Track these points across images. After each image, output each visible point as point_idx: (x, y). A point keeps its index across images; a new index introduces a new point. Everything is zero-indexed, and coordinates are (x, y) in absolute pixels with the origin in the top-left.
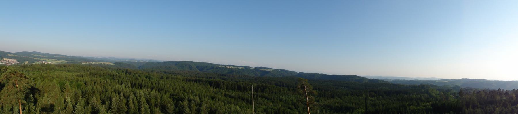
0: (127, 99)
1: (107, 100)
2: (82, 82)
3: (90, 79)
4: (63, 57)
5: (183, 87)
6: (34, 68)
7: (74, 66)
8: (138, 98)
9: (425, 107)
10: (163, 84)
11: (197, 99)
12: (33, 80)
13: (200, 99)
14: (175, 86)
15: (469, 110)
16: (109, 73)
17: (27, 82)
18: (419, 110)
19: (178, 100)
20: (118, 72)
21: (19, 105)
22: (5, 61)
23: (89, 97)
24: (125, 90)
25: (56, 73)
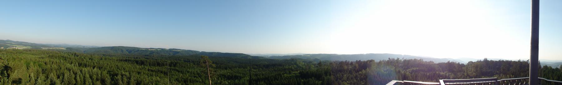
1: (61, 75)
3: (49, 60)
5: (117, 66)
6: (7, 52)
7: (36, 51)
8: (84, 74)
9: (295, 75)
10: (102, 64)
11: (127, 74)
12: (7, 60)
13: (129, 74)
15: (327, 77)
17: (2, 62)
18: (291, 76)
19: (113, 75)
20: (69, 55)
25: (23, 55)
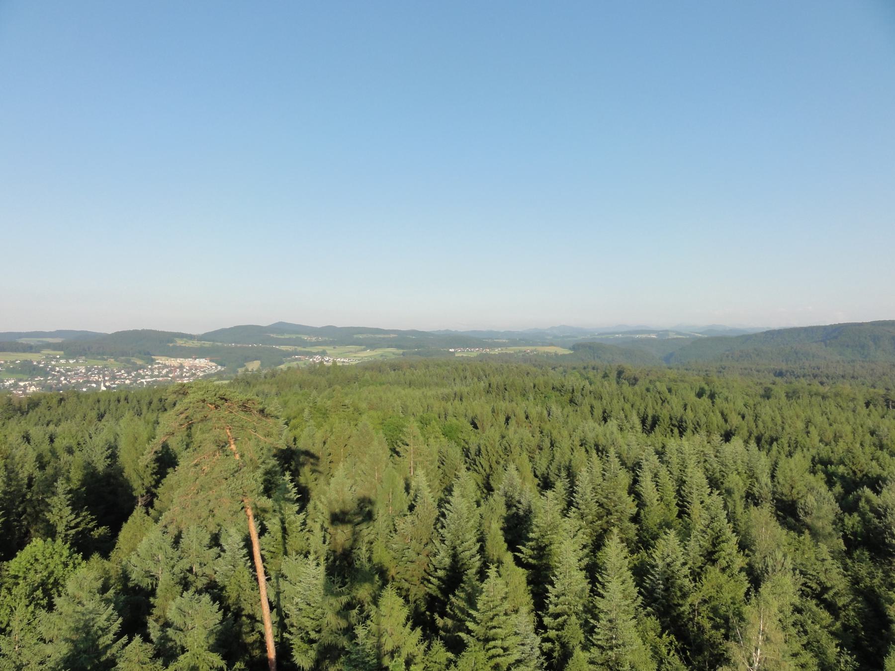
0: (634, 471)
2: (462, 419)
3: (488, 409)
4: (386, 336)
7: (427, 367)
12: (287, 424)
14: (831, 425)
16: (557, 384)
22: (166, 366)
23: (491, 466)
24: (621, 441)
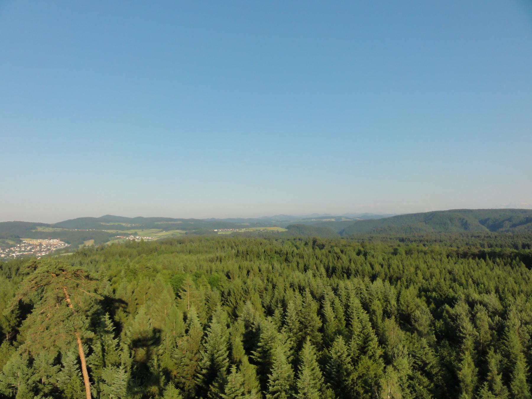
0: (320, 301)
2: (221, 273)
3: (237, 266)
7: (201, 241)
8: (344, 301)
12: (110, 280)
13: (501, 299)
14: (429, 269)
16: (278, 250)
17: (92, 289)
19: (439, 303)
21: (78, 345)
22: (30, 245)
23: (236, 302)
